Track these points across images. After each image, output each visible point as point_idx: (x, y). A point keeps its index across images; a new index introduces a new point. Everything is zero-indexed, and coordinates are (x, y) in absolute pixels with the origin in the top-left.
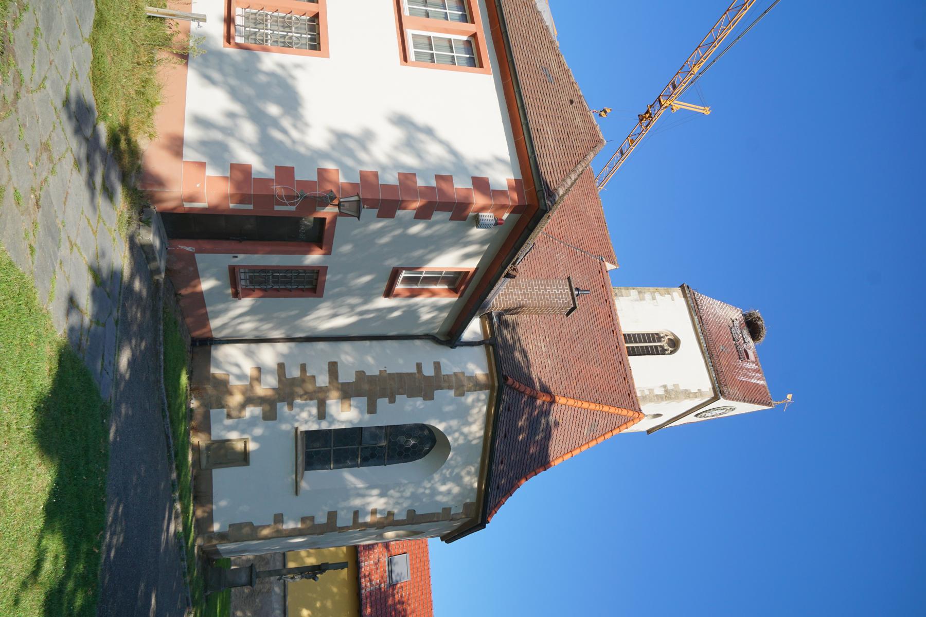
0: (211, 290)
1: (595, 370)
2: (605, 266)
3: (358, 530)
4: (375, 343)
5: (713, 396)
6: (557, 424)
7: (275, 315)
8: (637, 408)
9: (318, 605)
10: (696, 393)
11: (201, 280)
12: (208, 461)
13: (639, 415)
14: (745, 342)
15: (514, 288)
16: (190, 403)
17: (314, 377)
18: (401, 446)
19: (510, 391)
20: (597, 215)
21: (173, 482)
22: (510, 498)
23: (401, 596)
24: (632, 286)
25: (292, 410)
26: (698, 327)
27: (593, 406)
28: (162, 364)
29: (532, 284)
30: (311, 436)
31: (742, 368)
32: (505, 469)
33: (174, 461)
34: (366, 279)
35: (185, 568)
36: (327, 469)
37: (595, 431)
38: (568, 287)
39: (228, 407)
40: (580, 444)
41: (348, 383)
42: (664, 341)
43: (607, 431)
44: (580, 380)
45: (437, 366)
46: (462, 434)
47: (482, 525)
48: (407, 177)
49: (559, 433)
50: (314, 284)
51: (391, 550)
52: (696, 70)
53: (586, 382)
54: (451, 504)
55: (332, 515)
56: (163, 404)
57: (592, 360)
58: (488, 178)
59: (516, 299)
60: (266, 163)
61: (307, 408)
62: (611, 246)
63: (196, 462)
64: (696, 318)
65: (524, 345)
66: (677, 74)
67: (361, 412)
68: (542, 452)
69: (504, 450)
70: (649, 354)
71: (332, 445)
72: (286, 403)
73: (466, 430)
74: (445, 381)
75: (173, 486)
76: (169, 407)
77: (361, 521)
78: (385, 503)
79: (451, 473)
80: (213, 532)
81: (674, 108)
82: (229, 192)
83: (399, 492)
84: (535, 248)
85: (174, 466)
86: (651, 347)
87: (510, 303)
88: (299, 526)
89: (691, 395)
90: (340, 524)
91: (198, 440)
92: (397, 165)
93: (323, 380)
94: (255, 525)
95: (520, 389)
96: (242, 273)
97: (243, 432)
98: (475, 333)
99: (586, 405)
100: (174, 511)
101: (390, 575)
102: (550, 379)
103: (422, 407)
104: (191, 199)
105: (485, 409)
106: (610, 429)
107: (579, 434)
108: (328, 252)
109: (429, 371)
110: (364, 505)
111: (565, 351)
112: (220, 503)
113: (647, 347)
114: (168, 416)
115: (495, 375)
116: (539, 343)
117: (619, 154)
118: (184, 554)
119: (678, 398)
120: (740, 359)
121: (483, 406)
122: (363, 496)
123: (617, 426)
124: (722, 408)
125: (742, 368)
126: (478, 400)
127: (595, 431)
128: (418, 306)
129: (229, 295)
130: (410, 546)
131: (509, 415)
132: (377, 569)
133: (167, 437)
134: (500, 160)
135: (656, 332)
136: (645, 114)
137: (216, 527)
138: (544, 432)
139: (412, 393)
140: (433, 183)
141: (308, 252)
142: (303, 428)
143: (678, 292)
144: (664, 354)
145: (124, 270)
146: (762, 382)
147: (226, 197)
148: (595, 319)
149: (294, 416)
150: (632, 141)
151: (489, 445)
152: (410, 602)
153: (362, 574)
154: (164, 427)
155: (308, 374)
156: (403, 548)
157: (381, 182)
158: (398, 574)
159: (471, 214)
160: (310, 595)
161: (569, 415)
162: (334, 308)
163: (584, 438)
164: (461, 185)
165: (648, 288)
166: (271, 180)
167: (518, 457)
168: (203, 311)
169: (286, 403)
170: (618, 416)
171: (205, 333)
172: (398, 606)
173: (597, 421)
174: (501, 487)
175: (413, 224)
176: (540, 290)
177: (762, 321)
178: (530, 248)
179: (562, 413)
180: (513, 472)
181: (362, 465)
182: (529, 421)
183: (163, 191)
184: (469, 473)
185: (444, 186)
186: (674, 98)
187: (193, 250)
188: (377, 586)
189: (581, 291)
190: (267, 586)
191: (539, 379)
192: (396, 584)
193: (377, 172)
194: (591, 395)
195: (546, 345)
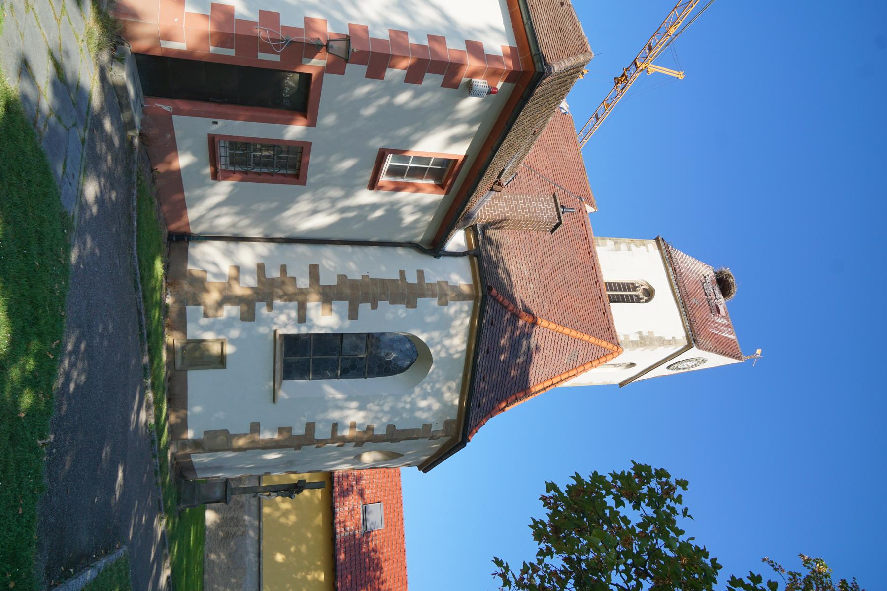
0: (188, 167)
2: (585, 206)
3: (337, 444)
4: (357, 249)
6: (537, 348)
7: (254, 207)
8: (616, 343)
9: (292, 549)
10: (670, 340)
11: (179, 153)
12: (183, 363)
13: (618, 348)
14: (716, 298)
15: (499, 201)
16: (166, 297)
17: (294, 278)
18: (381, 359)
19: (493, 303)
20: (576, 160)
21: (145, 368)
22: (491, 419)
23: (375, 544)
24: (608, 237)
25: (272, 311)
26: (672, 277)
27: (573, 333)
28: (135, 230)
29: (517, 198)
30: (289, 339)
31: (713, 321)
32: (486, 388)
33: (146, 342)
34: (348, 164)
35: (157, 466)
36: (306, 379)
37: (575, 361)
38: (553, 203)
39: (205, 306)
40: (560, 372)
41: (330, 286)
42: (639, 290)
43: (586, 362)
44: (561, 307)
45: (421, 274)
46: (444, 346)
47: (462, 444)
48: (399, 34)
49: (540, 358)
50: (297, 167)
51: (366, 499)
52: (672, 31)
53: (566, 310)
54: (431, 420)
55: (310, 427)
56: (135, 274)
57: (573, 290)
58: (481, 44)
59: (501, 211)
60: (249, 8)
61: (286, 311)
62: (590, 190)
63: (171, 363)
64: (670, 269)
65: (507, 266)
66: (654, 36)
67: (341, 318)
68: (523, 375)
69: (486, 366)
70: (624, 302)
71: (312, 354)
72: (265, 303)
73: (447, 342)
74: (428, 289)
75: (145, 371)
76: (142, 279)
77: (339, 434)
78: (364, 417)
79: (432, 388)
80: (187, 439)
81: (649, 70)
82: (209, 29)
83: (379, 405)
84: (517, 178)
85: (146, 348)
86: (627, 295)
87: (495, 215)
88: (276, 436)
89: (666, 343)
90: (318, 436)
91: (173, 339)
92: (387, 23)
93: (304, 282)
94: (231, 433)
95: (503, 303)
96: (223, 165)
97: (219, 332)
98: (459, 245)
99: (567, 331)
100: (146, 399)
101: (365, 522)
102: (532, 301)
103: (404, 315)
104: (167, 37)
105: (467, 321)
106: (590, 360)
107: (559, 361)
108: (312, 123)
109: (412, 278)
110: (342, 418)
111: (546, 278)
112: (195, 409)
113: (622, 295)
114: (141, 289)
115: (479, 285)
116: (521, 266)
117: (594, 119)
118: (157, 450)
120: (711, 313)
121: (465, 317)
122: (342, 408)
124: (694, 360)
125: (713, 321)
126: (461, 311)
128: (402, 204)
129: (206, 176)
130: (388, 482)
131: (492, 329)
132: (352, 515)
133: (140, 313)
134: (496, 30)
135: (632, 282)
136: (621, 78)
137: (190, 435)
138: (526, 354)
139: (395, 300)
140: (426, 43)
141: (289, 122)
142: (281, 332)
143: (652, 244)
145: (93, 93)
146: (732, 337)
147: (205, 38)
148: (576, 254)
149: (273, 319)
150: (608, 106)
151: (471, 358)
152: (383, 550)
153: (337, 520)
154: (136, 300)
155: (288, 276)
156: (377, 497)
157: (370, 36)
158: (372, 523)
159: (465, 80)
160: (284, 539)
161: (550, 340)
162: (314, 201)
163: (564, 367)
164: (454, 48)
165: (624, 239)
166: (255, 23)
167: (499, 377)
168: (177, 197)
169: (265, 303)
170: (598, 347)
171: (179, 227)
172: (372, 554)
173: (577, 350)
174: (482, 406)
175: (401, 90)
176: (525, 205)
177: (732, 278)
178: (512, 177)
179: (544, 336)
180: (494, 392)
181: (341, 377)
182: (511, 340)
183: (138, 22)
184: (450, 389)
185: (437, 47)
186: (650, 61)
187: (170, 109)
188: (352, 533)
189: (566, 209)
190: (242, 529)
191: (522, 301)
192: (370, 532)
193: (367, 26)
194: (572, 323)
195: (528, 269)
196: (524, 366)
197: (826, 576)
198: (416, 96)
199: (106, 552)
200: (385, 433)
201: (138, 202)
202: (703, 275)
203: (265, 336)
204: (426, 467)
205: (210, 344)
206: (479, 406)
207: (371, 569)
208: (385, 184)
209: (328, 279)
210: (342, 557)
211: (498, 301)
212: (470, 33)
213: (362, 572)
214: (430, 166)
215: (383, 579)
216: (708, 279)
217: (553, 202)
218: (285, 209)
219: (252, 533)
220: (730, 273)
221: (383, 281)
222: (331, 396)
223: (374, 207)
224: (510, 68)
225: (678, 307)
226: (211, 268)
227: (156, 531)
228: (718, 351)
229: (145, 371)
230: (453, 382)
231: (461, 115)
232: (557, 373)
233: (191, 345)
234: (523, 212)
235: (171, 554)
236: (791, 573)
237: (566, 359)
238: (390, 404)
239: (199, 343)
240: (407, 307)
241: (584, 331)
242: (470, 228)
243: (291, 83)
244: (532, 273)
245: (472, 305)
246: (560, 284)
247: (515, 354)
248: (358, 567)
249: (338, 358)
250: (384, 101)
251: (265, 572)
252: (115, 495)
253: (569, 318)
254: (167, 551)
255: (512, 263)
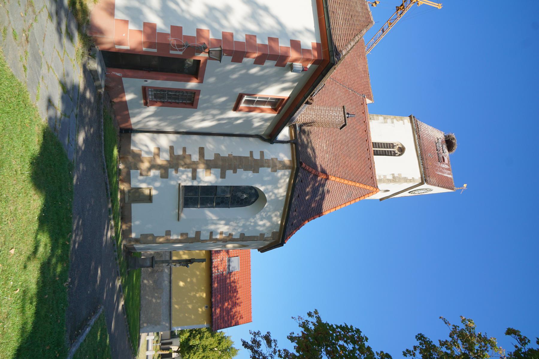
0: (131, 100)
4: (226, 138)
6: (328, 191)
7: (169, 117)
8: (376, 186)
9: (189, 280)
10: (411, 179)
11: (126, 94)
12: (129, 199)
14: (443, 152)
15: (310, 111)
17: (190, 155)
18: (239, 198)
19: (303, 171)
20: (364, 69)
23: (234, 279)
26: (417, 141)
27: (350, 183)
28: (103, 142)
29: (321, 109)
34: (223, 99)
38: (343, 112)
41: (210, 160)
43: (357, 198)
45: (262, 153)
46: (274, 193)
47: (282, 244)
48: (251, 37)
49: (329, 197)
50: (192, 100)
51: (230, 254)
54: (265, 231)
55: (198, 233)
58: (300, 41)
59: (311, 117)
60: (165, 24)
61: (186, 173)
63: (123, 199)
64: (416, 136)
65: (313, 145)
67: (217, 177)
70: (386, 155)
71: (199, 195)
72: (174, 169)
73: (276, 191)
74: (266, 163)
75: (110, 211)
76: (107, 167)
77: (214, 237)
80: (132, 238)
81: (419, 3)
82: (142, 40)
83: (236, 223)
86: (388, 151)
88: (180, 238)
89: (408, 181)
90: (202, 238)
91: (123, 187)
92: (245, 29)
93: (195, 157)
97: (149, 184)
98: (285, 136)
99: (346, 182)
103: (252, 176)
104: (120, 43)
105: (288, 180)
108: (201, 82)
109: (257, 156)
112: (136, 223)
113: (385, 151)
115: (295, 161)
117: (381, 32)
120: (439, 161)
121: (286, 178)
122: (216, 224)
123: (363, 195)
126: (284, 175)
132: (222, 263)
133: (106, 184)
136: (400, 7)
137: (133, 235)
140: (267, 42)
141: (189, 81)
142: (183, 184)
144: (395, 156)
146: (450, 176)
147: (141, 43)
149: (178, 177)
150: (390, 24)
151: (289, 200)
153: (213, 266)
154: (104, 178)
156: (236, 253)
157: (234, 40)
158: (233, 267)
159: (288, 63)
160: (184, 274)
161: (336, 187)
162: (203, 116)
164: (283, 44)
166: (168, 34)
168: (126, 113)
169: (174, 169)
172: (232, 284)
174: (294, 224)
175: (252, 67)
176: (325, 113)
182: (313, 189)
184: (276, 216)
185: (273, 44)
188: (221, 273)
189: (351, 115)
191: (320, 165)
196: (319, 202)
197: (473, 329)
198: (262, 70)
199: (94, 313)
200: (239, 238)
201: (104, 126)
202: (437, 138)
203: (174, 186)
204: (262, 250)
205: (143, 190)
206: (292, 225)
207: (232, 292)
208: (242, 108)
209: (209, 156)
210: (216, 285)
211: (306, 170)
212: (293, 34)
213: (226, 293)
214: (269, 100)
215: (238, 297)
216: (440, 141)
217: (343, 111)
218: (186, 119)
219: (166, 271)
220: (454, 136)
221: (240, 158)
222: (210, 218)
223: (237, 119)
224: (316, 57)
225: (418, 159)
226: (145, 148)
227: (116, 286)
228: (440, 185)
229: (110, 211)
230: (277, 212)
231: (287, 79)
232: (339, 204)
233: (133, 191)
234: (324, 118)
235: (124, 294)
236: (454, 326)
237: (345, 197)
238: (243, 222)
239: (138, 189)
240: (253, 172)
241: (357, 181)
242: (292, 126)
243: (188, 62)
244: (328, 148)
245: (290, 172)
246: (345, 153)
247: (315, 195)
248: (224, 291)
249: (214, 197)
250: (243, 72)
251: (173, 292)
252: (97, 283)
253: (348, 174)
254: (122, 293)
255: (317, 143)
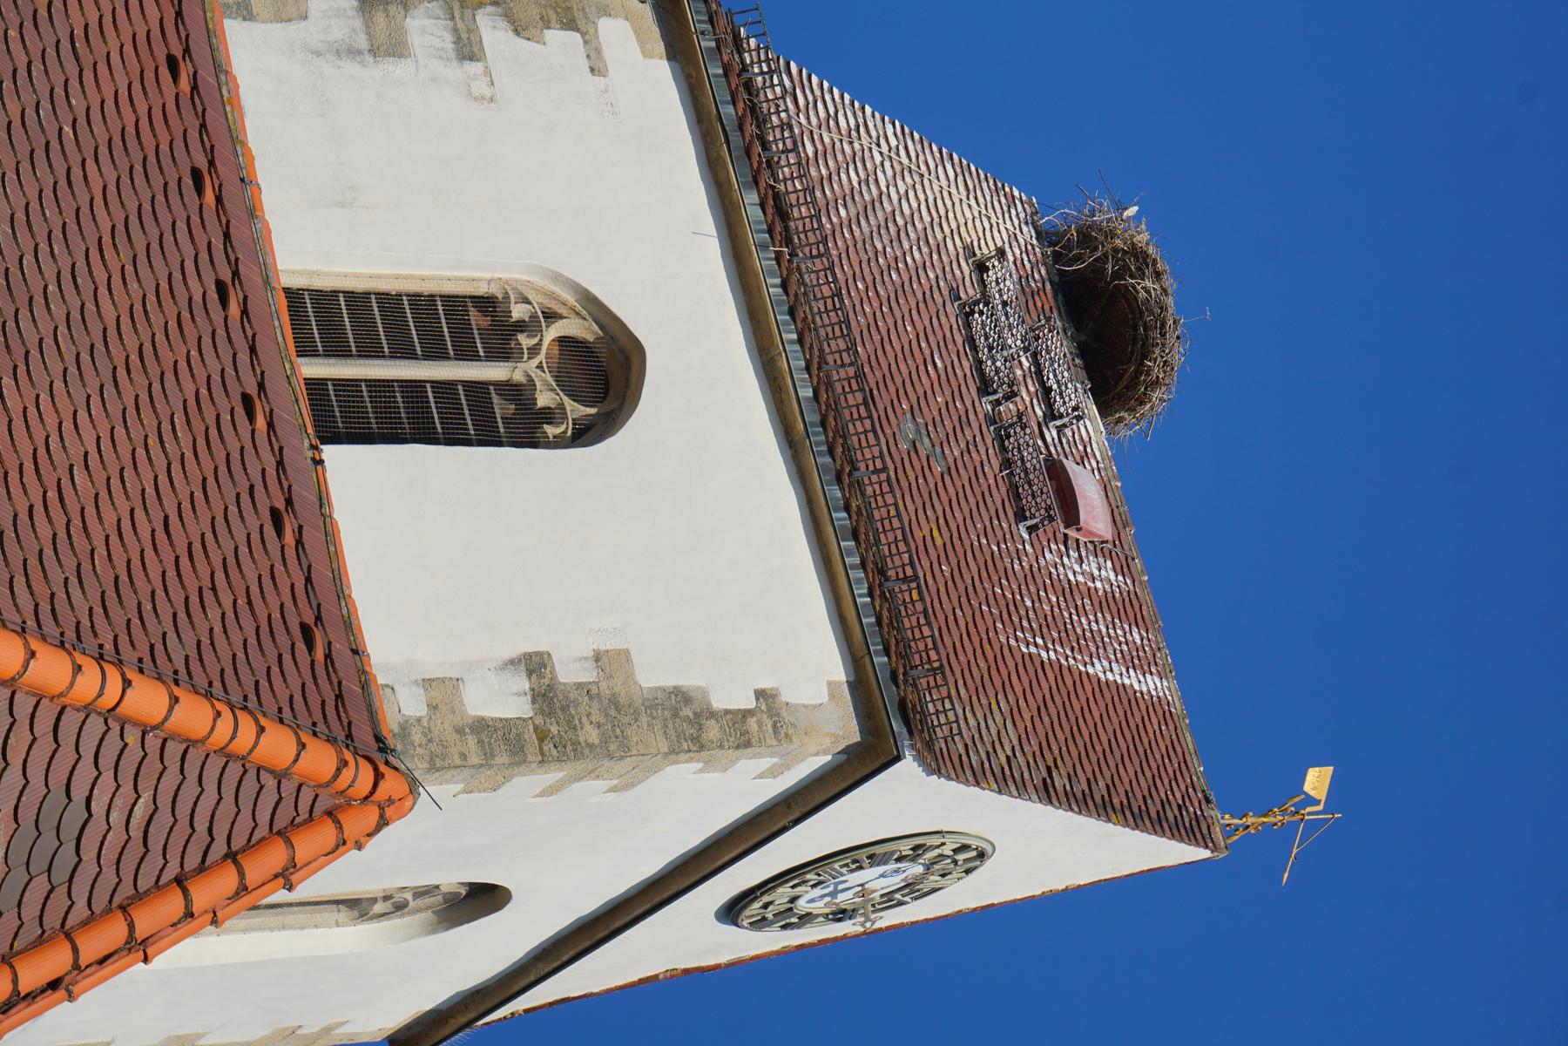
1: (68, 425)
5: (856, 738)
8: (363, 735)
10: (746, 714)
13: (378, 776)
14: (1051, 415)
26: (762, 262)
42: (534, 350)
43: (145, 882)
70: (426, 436)
86: (445, 388)
89: (713, 731)
106: (172, 870)
113: (414, 388)
119: (625, 748)
120: (1021, 516)
123: (219, 849)
124: (905, 848)
127: (61, 875)
135: (482, 290)
144: (534, 445)
146: (1151, 685)
170: (234, 770)
173: (79, 793)
202: (969, 251)
241: (127, 653)
